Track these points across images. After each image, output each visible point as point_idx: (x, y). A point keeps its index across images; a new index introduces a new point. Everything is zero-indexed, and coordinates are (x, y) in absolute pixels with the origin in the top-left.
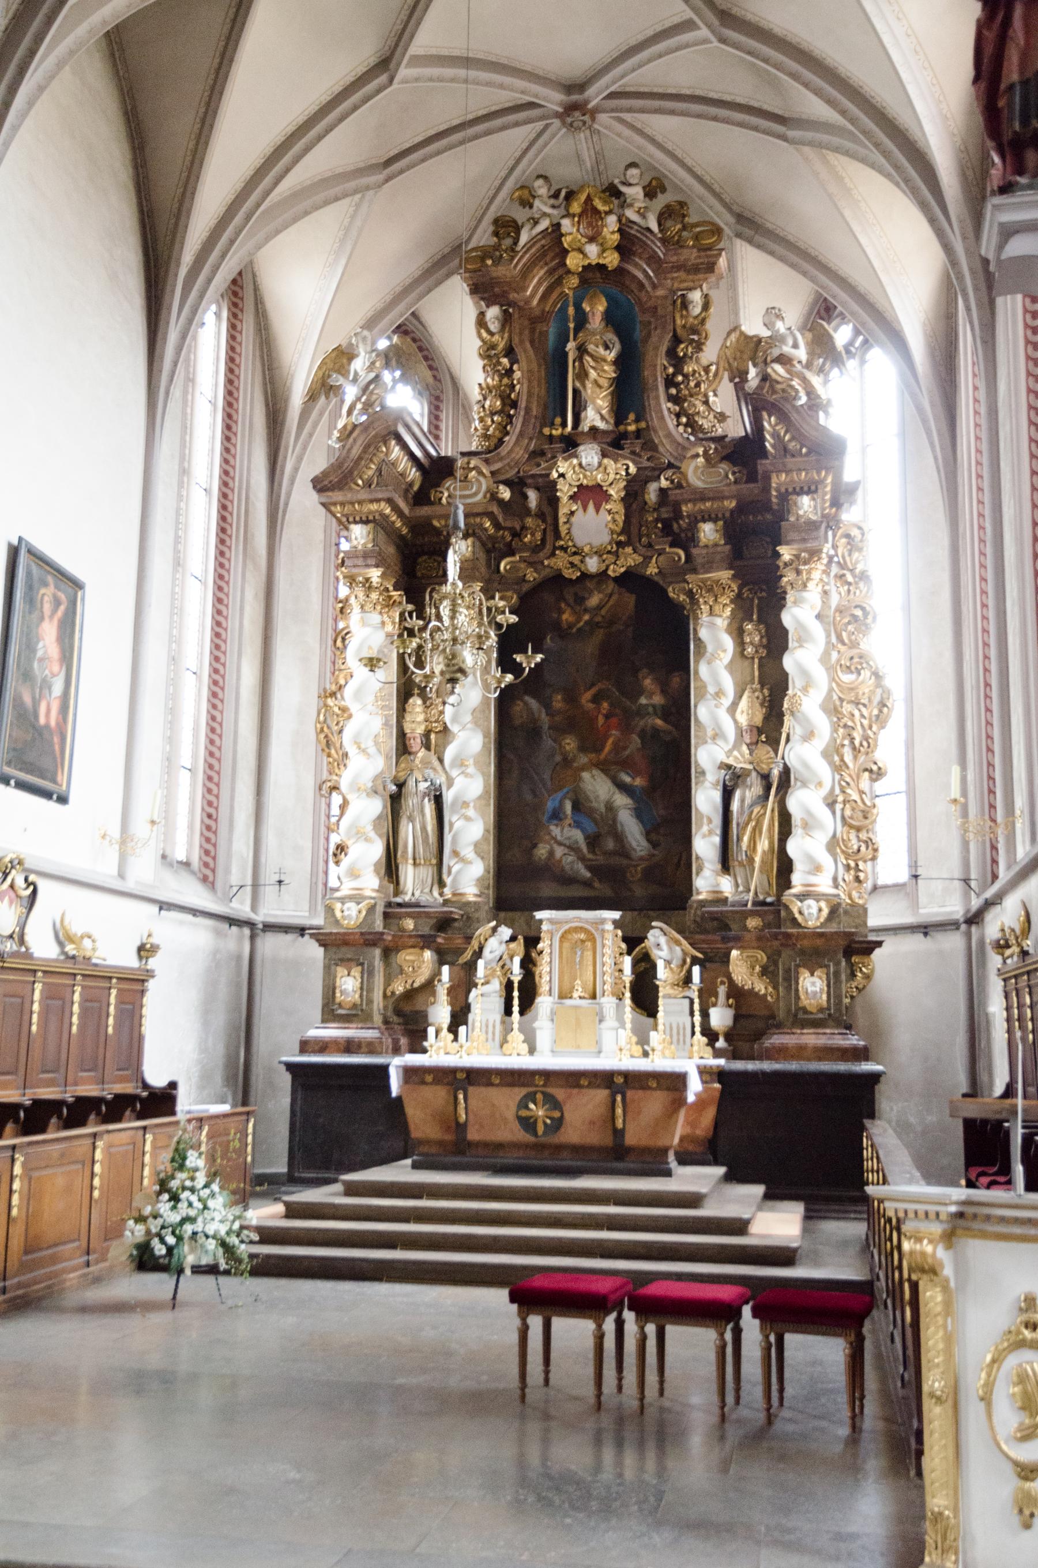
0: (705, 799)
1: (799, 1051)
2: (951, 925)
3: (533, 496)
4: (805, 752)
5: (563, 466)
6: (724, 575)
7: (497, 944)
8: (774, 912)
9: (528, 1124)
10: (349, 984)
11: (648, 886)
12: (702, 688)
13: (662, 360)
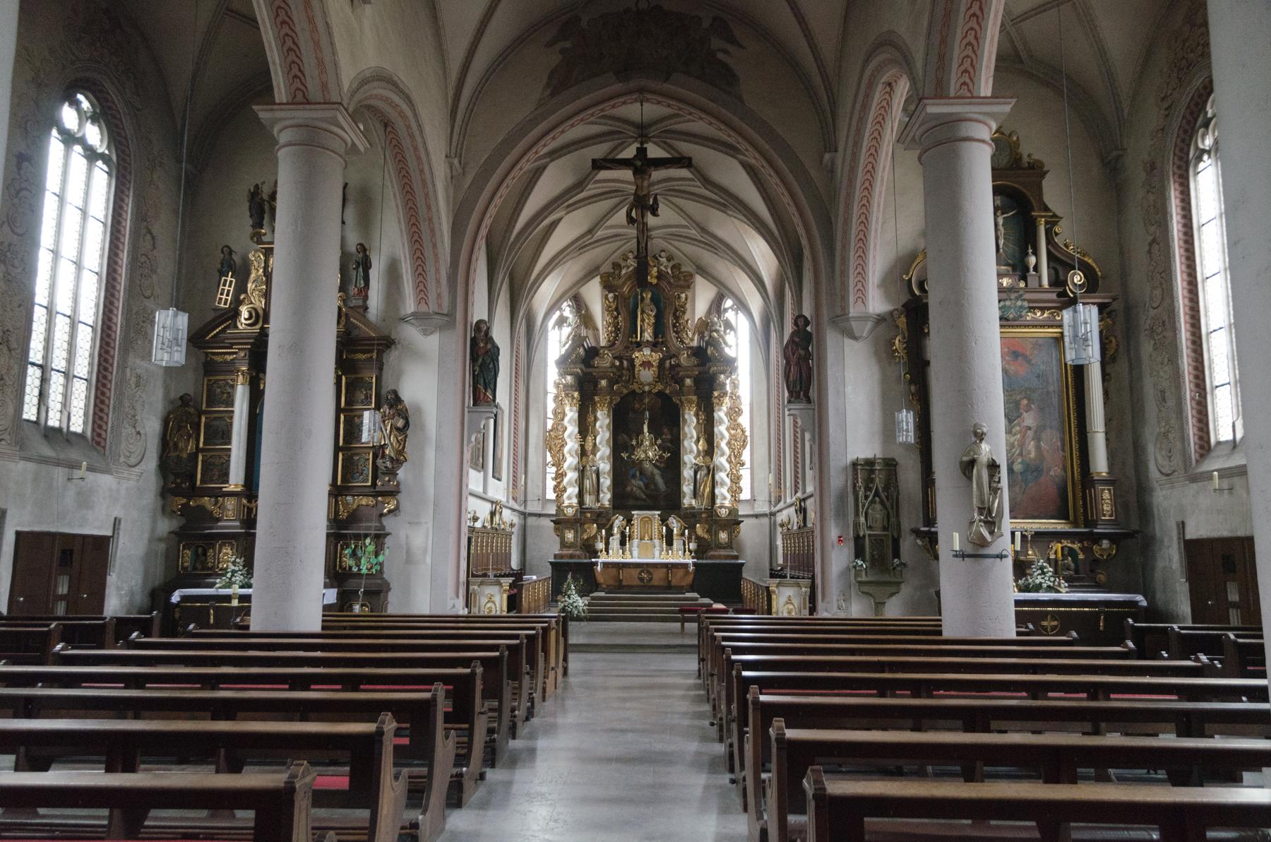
0: (687, 473)
1: (717, 557)
2: (764, 515)
3: (625, 363)
4: (721, 460)
5: (637, 354)
6: (695, 398)
7: (618, 521)
8: (711, 510)
9: (642, 579)
10: (570, 536)
11: (668, 502)
12: (685, 435)
13: (671, 318)
